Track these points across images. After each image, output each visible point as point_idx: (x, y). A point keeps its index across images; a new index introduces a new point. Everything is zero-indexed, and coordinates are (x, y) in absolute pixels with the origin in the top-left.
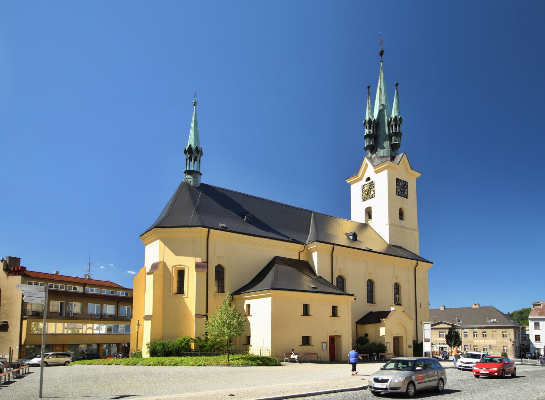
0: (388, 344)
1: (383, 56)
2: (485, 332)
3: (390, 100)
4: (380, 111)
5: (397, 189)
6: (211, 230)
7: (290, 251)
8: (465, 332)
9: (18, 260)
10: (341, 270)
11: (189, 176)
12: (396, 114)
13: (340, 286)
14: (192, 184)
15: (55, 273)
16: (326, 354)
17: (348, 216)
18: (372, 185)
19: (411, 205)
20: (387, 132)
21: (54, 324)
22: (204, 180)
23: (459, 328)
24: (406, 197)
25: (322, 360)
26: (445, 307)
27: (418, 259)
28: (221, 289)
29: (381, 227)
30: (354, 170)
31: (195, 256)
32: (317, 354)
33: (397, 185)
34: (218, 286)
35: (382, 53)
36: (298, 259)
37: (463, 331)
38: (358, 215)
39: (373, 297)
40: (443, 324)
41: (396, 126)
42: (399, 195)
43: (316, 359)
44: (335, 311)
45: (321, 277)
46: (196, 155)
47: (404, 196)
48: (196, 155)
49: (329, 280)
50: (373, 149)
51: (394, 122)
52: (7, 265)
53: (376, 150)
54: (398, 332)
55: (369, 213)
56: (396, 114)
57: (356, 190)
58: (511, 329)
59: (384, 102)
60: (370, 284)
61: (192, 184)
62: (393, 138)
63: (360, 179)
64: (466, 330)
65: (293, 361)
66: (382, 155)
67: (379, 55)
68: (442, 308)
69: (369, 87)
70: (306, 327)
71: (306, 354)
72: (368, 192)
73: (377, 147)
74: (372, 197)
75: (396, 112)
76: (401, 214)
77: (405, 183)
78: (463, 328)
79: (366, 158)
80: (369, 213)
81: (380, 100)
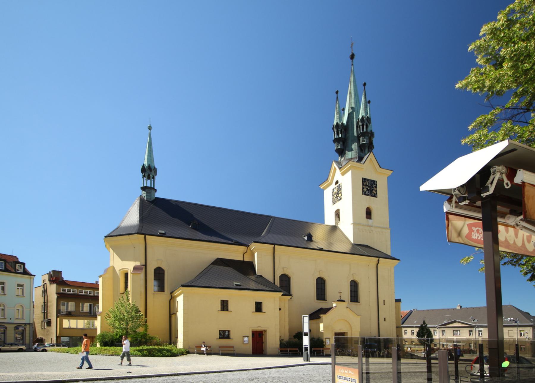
0: (327, 340)
1: (354, 60)
2: (481, 331)
3: (358, 102)
4: (349, 114)
5: (363, 188)
6: (276, 246)
7: (234, 253)
8: (443, 331)
9: (60, 272)
10: (285, 269)
11: (144, 192)
12: (364, 114)
13: (285, 285)
14: (145, 198)
15: (95, 282)
16: (249, 348)
17: (323, 221)
18: (339, 188)
19: (380, 204)
20: (355, 134)
21: (75, 321)
22: (158, 195)
23: (474, 327)
24: (375, 196)
25: (237, 352)
26: (461, 307)
27: (380, 255)
28: (161, 288)
29: (347, 227)
30: (324, 177)
31: (135, 260)
32: (233, 347)
33: (363, 185)
34: (159, 286)
35: (352, 57)
36: (242, 259)
37: (477, 329)
38: (329, 220)
39: (357, 297)
40: (457, 323)
41: (363, 126)
42: (365, 195)
43: (232, 352)
44: (259, 307)
45: (261, 276)
46: (149, 173)
47: (372, 196)
48: (149, 173)
49: (270, 279)
50: (341, 152)
51: (361, 122)
52: (51, 277)
53: (345, 153)
54: (340, 328)
55: (337, 214)
56: (364, 114)
57: (328, 194)
58: (529, 328)
59: (353, 105)
60: (321, 283)
61: (145, 198)
62: (361, 138)
63: (331, 184)
64: (480, 329)
65: (202, 353)
66: (350, 157)
67: (349, 59)
68: (458, 308)
69: (337, 92)
70: (224, 321)
71: (220, 347)
72: (337, 196)
73: (346, 150)
74: (340, 199)
75: (364, 112)
76: (369, 214)
77: (374, 183)
78: (478, 327)
79: (334, 162)
80: (337, 214)
81: (350, 103)
